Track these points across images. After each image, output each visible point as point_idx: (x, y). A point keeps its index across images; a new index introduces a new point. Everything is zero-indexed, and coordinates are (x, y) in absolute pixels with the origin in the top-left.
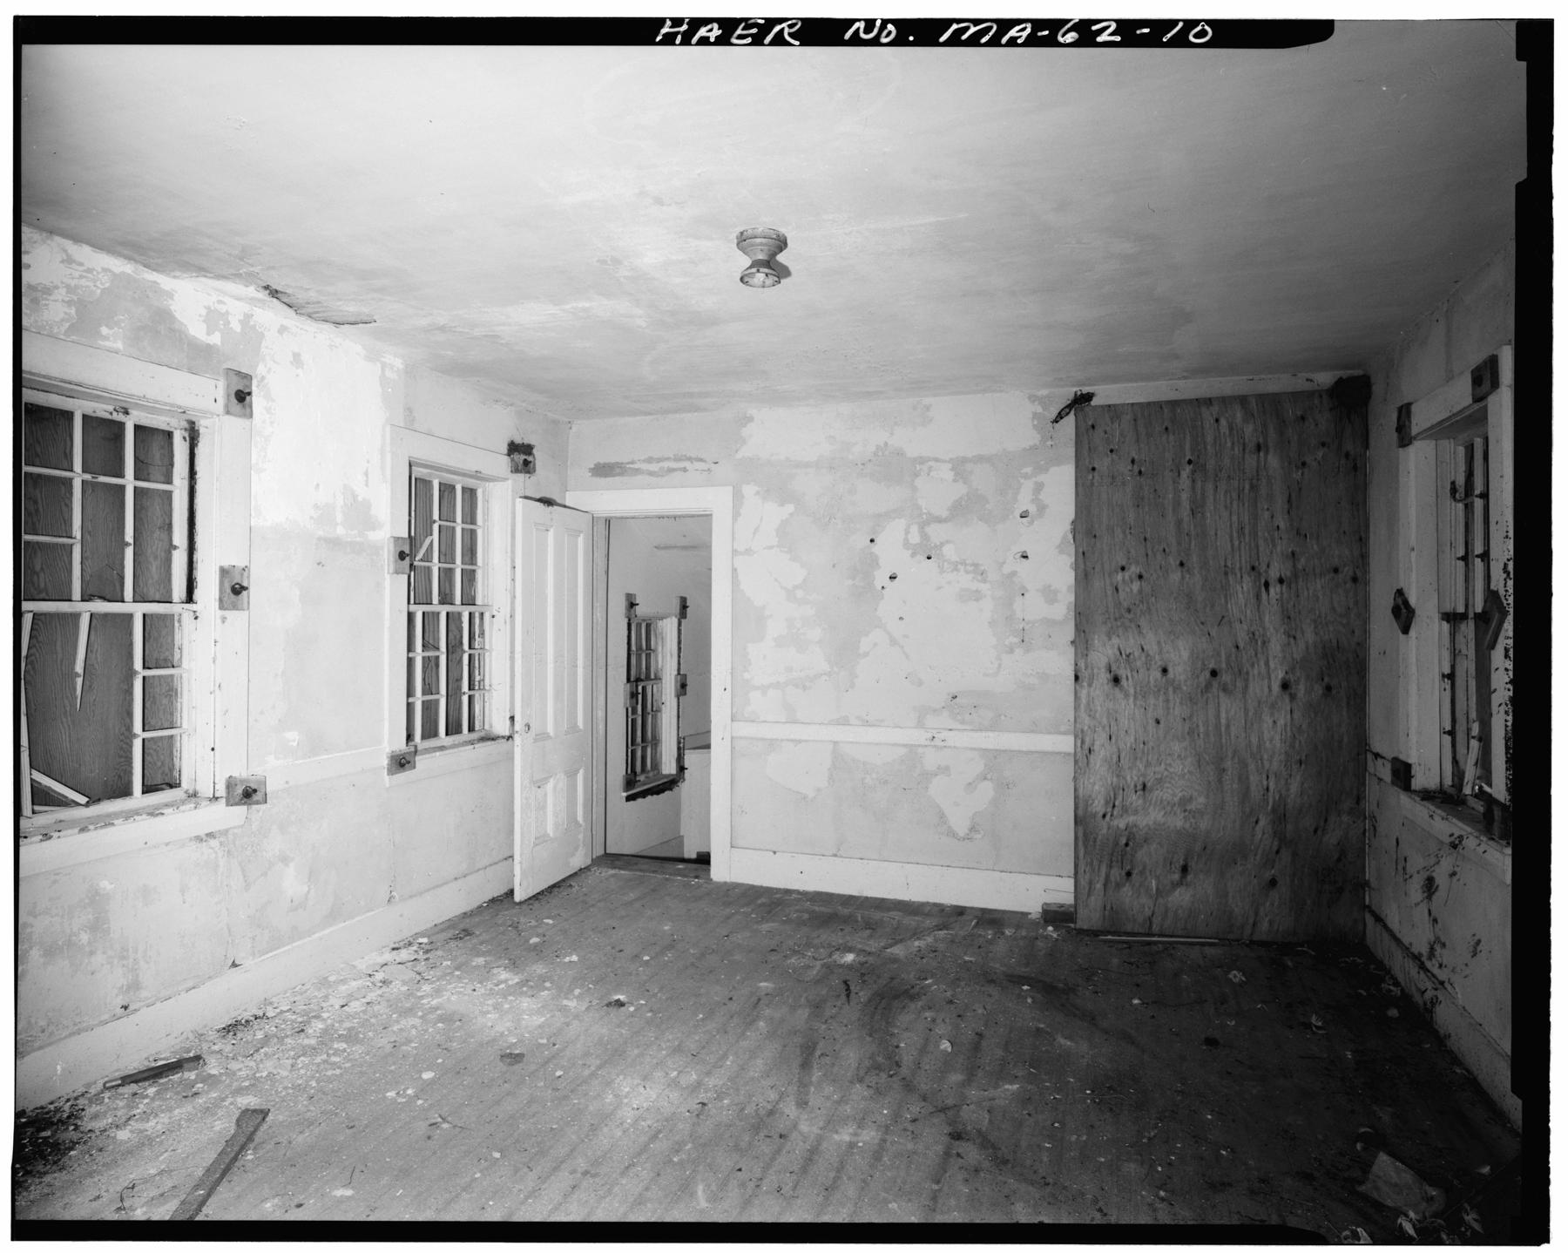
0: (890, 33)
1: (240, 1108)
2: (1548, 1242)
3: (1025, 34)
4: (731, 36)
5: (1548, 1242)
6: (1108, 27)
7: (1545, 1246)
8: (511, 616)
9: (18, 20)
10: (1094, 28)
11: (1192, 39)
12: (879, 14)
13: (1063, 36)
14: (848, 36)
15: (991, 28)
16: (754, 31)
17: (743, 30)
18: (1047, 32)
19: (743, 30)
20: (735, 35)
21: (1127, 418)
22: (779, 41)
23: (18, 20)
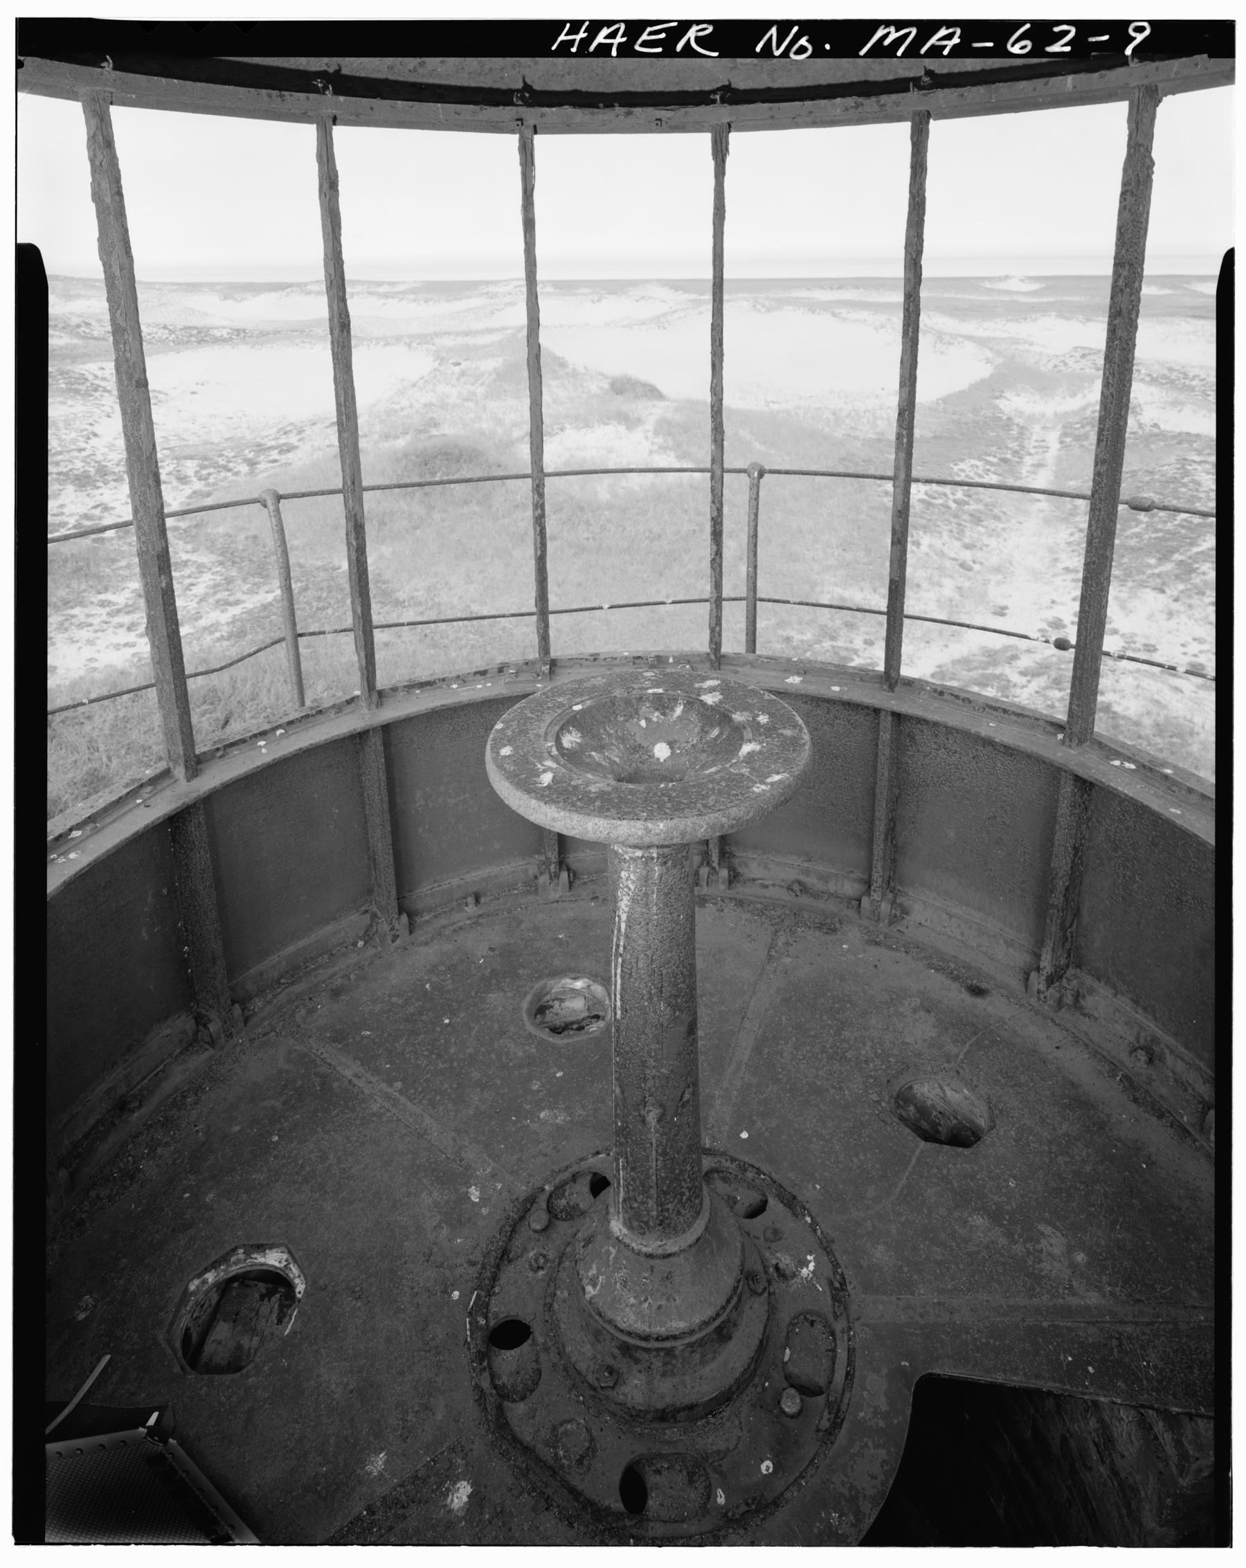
0: (1022, 48)
1: (120, 461)
2: (16, 1544)
3: (950, 43)
4: (634, 43)
5: (16, 1544)
6: (908, 34)
7: (12, 1540)
8: (848, 1374)
9: (1220, 1536)
10: (1056, 29)
11: (637, 48)
12: (674, 12)
13: (1013, 45)
14: (679, 47)
15: (1068, 32)
16: (663, 36)
17: (566, 35)
18: (1106, 38)
19: (566, 35)
20: (640, 41)
21: (22, 58)
22: (688, 52)
23: (1220, 1536)
